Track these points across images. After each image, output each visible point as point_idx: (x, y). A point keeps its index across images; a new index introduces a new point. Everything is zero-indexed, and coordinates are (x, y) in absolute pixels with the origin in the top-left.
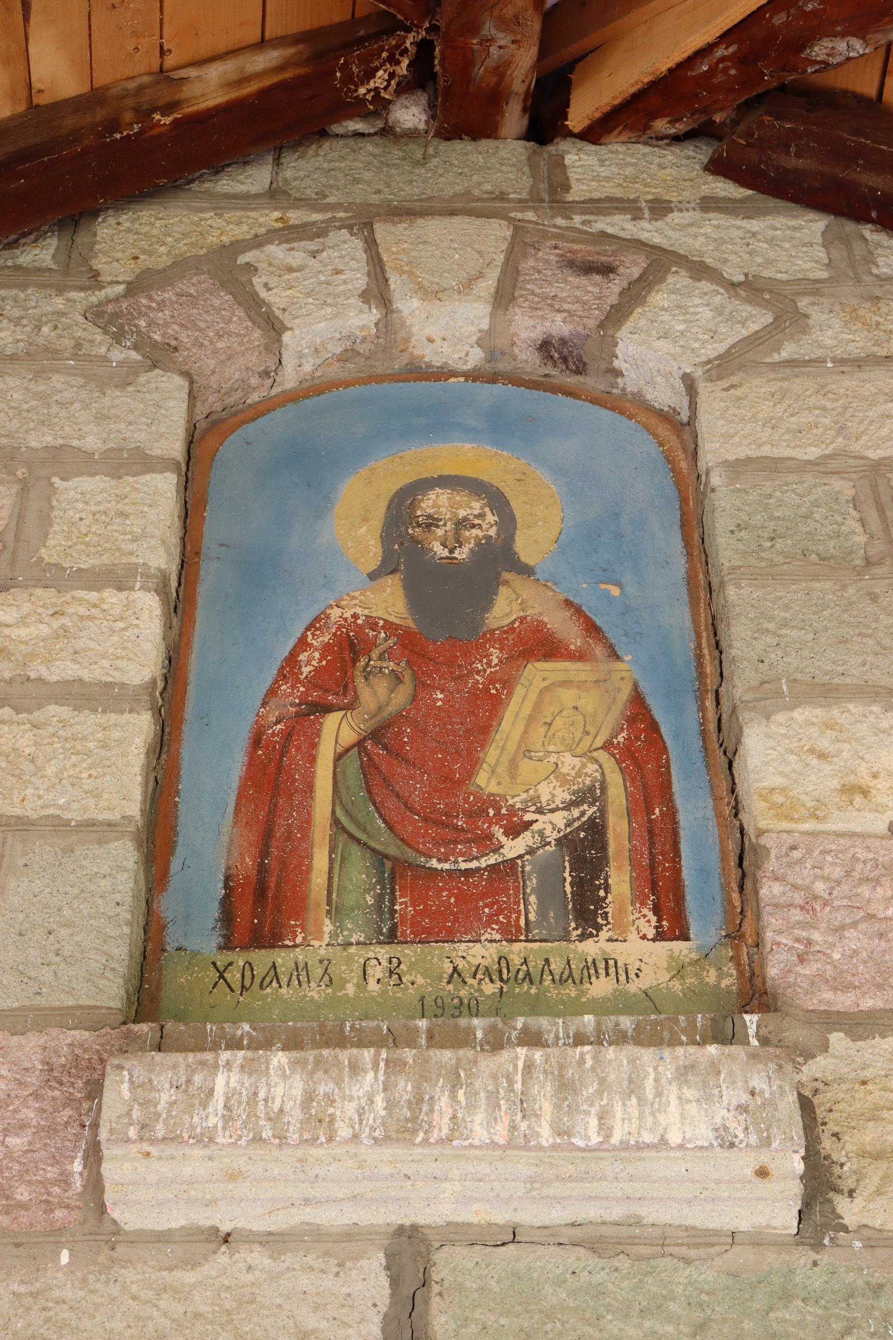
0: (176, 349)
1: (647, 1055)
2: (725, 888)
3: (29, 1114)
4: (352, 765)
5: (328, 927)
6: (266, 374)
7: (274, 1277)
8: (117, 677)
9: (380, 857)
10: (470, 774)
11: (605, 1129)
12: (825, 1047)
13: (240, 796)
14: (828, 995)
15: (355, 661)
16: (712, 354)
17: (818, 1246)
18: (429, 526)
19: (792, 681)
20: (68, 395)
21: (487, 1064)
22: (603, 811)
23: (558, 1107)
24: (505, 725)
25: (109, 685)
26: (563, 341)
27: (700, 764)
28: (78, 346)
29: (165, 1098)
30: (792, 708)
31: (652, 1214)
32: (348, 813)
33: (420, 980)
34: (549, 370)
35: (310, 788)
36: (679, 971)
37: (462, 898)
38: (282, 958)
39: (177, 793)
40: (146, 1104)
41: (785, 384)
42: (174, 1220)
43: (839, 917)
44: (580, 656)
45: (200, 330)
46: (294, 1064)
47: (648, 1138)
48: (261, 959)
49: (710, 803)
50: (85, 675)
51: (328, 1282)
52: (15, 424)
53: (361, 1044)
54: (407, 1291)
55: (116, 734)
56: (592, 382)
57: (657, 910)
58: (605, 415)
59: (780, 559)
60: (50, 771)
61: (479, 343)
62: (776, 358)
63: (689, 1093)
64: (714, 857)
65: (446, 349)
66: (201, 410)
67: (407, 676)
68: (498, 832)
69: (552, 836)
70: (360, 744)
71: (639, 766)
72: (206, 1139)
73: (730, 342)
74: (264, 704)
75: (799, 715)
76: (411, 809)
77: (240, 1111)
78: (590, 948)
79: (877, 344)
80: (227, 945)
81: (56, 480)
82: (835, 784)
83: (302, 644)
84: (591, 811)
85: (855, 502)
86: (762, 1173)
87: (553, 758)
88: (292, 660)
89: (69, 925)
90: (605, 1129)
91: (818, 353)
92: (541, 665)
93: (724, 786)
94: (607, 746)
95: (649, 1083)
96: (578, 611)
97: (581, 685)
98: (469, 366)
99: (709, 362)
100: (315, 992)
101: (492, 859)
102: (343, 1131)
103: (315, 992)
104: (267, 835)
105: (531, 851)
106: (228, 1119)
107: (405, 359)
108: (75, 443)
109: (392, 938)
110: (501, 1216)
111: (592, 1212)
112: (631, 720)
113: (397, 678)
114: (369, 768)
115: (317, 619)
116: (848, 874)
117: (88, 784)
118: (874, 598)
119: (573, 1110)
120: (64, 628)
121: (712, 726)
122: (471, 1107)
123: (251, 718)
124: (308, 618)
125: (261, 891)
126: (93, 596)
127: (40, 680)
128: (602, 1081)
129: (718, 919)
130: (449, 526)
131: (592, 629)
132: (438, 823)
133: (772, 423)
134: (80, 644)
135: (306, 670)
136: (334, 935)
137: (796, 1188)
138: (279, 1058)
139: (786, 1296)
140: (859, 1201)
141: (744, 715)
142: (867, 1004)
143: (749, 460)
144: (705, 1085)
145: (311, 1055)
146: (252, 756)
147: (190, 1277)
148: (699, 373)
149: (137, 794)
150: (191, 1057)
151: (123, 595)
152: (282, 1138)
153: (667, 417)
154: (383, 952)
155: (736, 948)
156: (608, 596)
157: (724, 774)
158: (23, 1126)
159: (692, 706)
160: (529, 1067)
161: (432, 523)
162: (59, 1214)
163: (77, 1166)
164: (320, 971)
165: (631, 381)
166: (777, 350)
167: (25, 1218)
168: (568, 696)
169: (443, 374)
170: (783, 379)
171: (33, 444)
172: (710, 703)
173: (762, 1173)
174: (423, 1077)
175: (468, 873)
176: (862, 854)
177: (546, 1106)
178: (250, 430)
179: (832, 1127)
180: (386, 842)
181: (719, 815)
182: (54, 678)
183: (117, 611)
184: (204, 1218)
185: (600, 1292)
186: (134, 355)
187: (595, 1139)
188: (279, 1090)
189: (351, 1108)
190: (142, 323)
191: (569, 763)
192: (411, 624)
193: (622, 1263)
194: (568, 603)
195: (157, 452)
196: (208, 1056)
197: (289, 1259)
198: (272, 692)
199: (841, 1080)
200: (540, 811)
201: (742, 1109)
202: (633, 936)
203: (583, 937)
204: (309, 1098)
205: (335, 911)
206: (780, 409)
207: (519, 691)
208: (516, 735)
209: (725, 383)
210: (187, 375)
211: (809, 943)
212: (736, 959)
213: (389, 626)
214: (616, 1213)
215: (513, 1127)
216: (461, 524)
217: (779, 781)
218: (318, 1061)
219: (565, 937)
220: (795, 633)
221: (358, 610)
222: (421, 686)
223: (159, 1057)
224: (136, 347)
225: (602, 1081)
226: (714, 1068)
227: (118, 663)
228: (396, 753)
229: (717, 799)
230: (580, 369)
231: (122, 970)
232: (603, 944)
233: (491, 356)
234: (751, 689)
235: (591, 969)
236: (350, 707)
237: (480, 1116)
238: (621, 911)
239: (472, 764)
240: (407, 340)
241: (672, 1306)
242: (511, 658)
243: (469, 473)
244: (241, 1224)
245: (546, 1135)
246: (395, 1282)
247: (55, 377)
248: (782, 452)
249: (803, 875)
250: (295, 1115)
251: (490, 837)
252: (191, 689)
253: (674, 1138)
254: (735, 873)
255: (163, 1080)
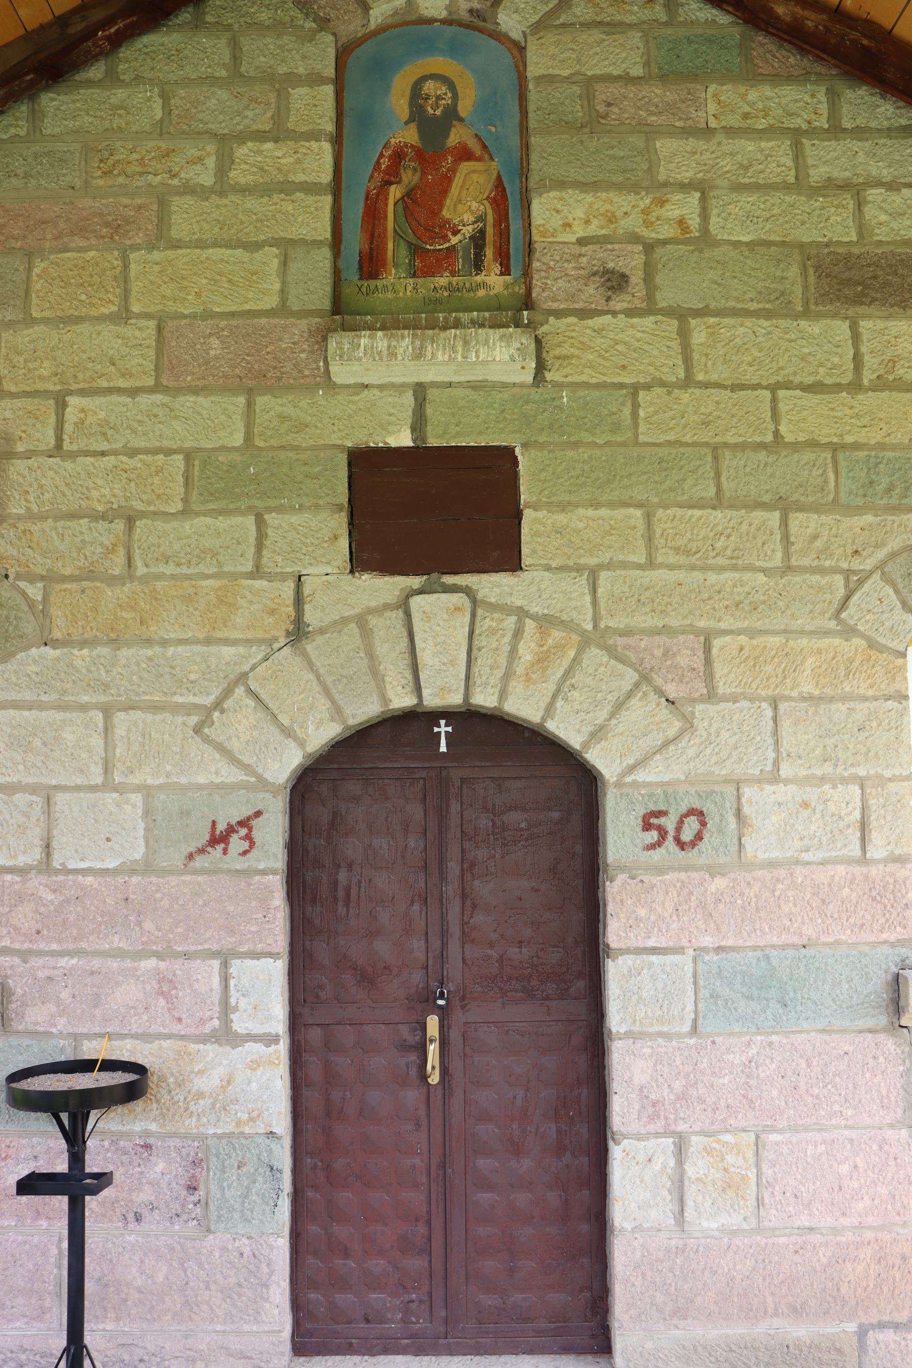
0: (329, 20)
1: (491, 331)
2: (524, 256)
3: (305, 346)
4: (400, 207)
5: (393, 271)
6: (364, 25)
7: (381, 398)
8: (318, 180)
9: (410, 244)
10: (440, 210)
11: (477, 356)
12: (547, 322)
13: (363, 220)
14: (550, 304)
15: (400, 162)
16: (534, 21)
17: (538, 387)
18: (426, 99)
19: (551, 180)
20: (290, 46)
21: (443, 335)
22: (485, 225)
23: (463, 349)
24: (453, 189)
25: (316, 184)
26: (478, 10)
27: (519, 206)
28: (292, 20)
29: (346, 347)
30: (549, 192)
31: (490, 378)
32: (399, 227)
33: (424, 291)
34: (472, 19)
35: (386, 216)
36: (507, 287)
37: (437, 260)
38: (379, 283)
39: (341, 219)
40: (341, 349)
41: (560, 37)
42: (351, 381)
43: (558, 275)
44: (479, 159)
45: (338, 10)
46: (385, 335)
47: (490, 359)
48: (372, 283)
49: (521, 222)
50: (308, 180)
51: (396, 399)
52: (272, 62)
53: (405, 328)
54: (419, 402)
55: (320, 205)
56: (490, 26)
57: (501, 264)
58: (493, 42)
59: (551, 124)
60: (299, 220)
61: (446, 9)
62: (558, 22)
63: (503, 344)
64: (521, 243)
65: (433, 11)
66: (340, 44)
67: (419, 170)
68: (450, 234)
69: (468, 235)
70: (402, 198)
71: (497, 205)
72: (359, 359)
73: (541, 14)
74: (369, 181)
75: (552, 194)
76: (420, 225)
77: (369, 351)
78: (479, 279)
79: (597, 15)
80: (361, 278)
81: (290, 89)
82: (561, 223)
83: (381, 155)
84: (481, 225)
85: (580, 97)
86: (523, 368)
87: (469, 203)
88: (378, 163)
89: (311, 280)
90: (477, 356)
91: (574, 20)
92: (466, 163)
93: (526, 215)
94: (488, 198)
95: (491, 341)
96: (480, 139)
97: (480, 172)
98: (442, 17)
99: (532, 25)
100: (390, 295)
101: (447, 245)
102: (400, 358)
103: (390, 295)
104: (372, 236)
105: (460, 242)
106: (365, 354)
107: (417, 15)
108: (295, 71)
109: (414, 276)
110: (447, 379)
111: (473, 378)
112: (496, 187)
113: (415, 170)
114: (406, 208)
115: (386, 144)
116: (561, 258)
117: (312, 225)
118: (582, 142)
119: (468, 350)
120: (298, 158)
121: (524, 189)
122: (438, 349)
123: (365, 188)
124: (383, 144)
125: (371, 258)
126: (307, 144)
127: (293, 182)
128: (477, 340)
129: (521, 267)
130: (434, 99)
131: (484, 147)
132: (430, 231)
133: (553, 57)
134: (305, 166)
135: (383, 166)
136: (395, 274)
137: (533, 371)
138: (380, 334)
139: (527, 402)
140: (552, 373)
141: (533, 195)
142: (562, 306)
143: (543, 76)
144: (508, 342)
145: (389, 332)
146: (366, 204)
147: (357, 398)
148: (528, 31)
149: (329, 229)
150: (353, 333)
151: (318, 144)
152: (381, 359)
153: (516, 44)
154: (411, 281)
155: (526, 279)
156: (490, 132)
157: (526, 211)
158: (304, 351)
159: (518, 181)
160: (455, 336)
161: (428, 97)
162: (318, 379)
163: (321, 364)
164: (391, 288)
165: (504, 28)
166: (559, 18)
167: (308, 380)
168: (475, 177)
169: (430, 21)
170: (560, 34)
171: (280, 72)
172: (524, 180)
173: (523, 368)
174: (423, 340)
175: (440, 250)
176: (566, 251)
177: (460, 349)
178: (358, 51)
179: (547, 349)
180: (412, 238)
181: (524, 227)
182: (297, 181)
183: (316, 150)
184: (360, 381)
185: (475, 401)
186: (314, 25)
187: (474, 359)
188: (380, 344)
189: (402, 350)
190: (315, 7)
191: (474, 205)
192: (420, 145)
193: (482, 393)
194: (476, 135)
195: (325, 75)
196: (358, 333)
197: (385, 393)
198: (372, 176)
199: (551, 333)
200: (464, 225)
201: (518, 349)
202: (493, 274)
203: (476, 275)
204: (389, 347)
205: (396, 265)
206: (557, 50)
207: (458, 175)
208: (456, 194)
209: (537, 36)
210: (334, 34)
211: (546, 284)
212: (525, 283)
213: (412, 146)
214: (480, 378)
215: (450, 356)
216: (439, 98)
217: (542, 222)
218: (391, 334)
219: (471, 275)
220: (553, 158)
221: (401, 139)
222: (424, 174)
223: (343, 333)
224: (314, 21)
225: (477, 340)
226: (511, 336)
227: (320, 174)
228: (415, 201)
229: (524, 220)
230: (484, 20)
231: (329, 296)
232: (483, 277)
233: (450, 13)
234: (537, 183)
235: (479, 286)
236: (399, 182)
237: (440, 353)
238: (489, 265)
239: (441, 206)
240: (418, 8)
241: (495, 405)
242: (455, 160)
243: (441, 72)
244: (371, 382)
245: (460, 358)
246: (416, 399)
247: (285, 37)
248: (557, 72)
249: (546, 259)
250: (385, 353)
251: (447, 236)
252: (343, 175)
253: (498, 359)
254: (527, 250)
255: (345, 341)
